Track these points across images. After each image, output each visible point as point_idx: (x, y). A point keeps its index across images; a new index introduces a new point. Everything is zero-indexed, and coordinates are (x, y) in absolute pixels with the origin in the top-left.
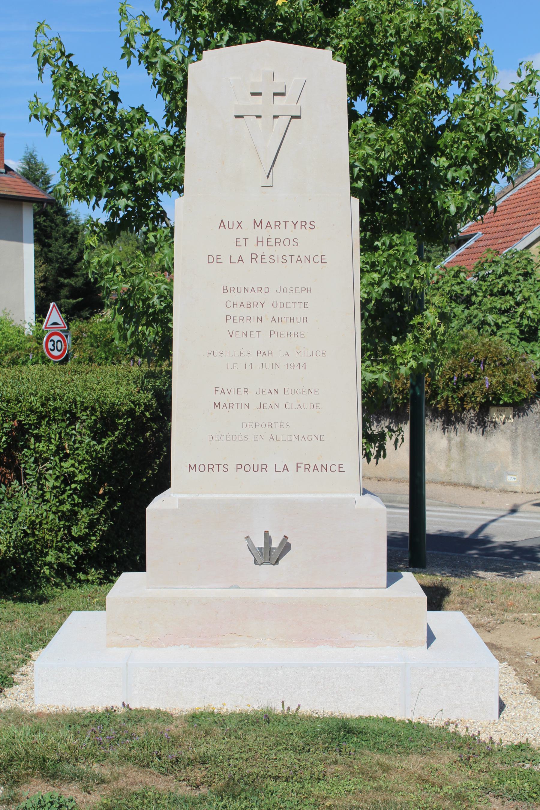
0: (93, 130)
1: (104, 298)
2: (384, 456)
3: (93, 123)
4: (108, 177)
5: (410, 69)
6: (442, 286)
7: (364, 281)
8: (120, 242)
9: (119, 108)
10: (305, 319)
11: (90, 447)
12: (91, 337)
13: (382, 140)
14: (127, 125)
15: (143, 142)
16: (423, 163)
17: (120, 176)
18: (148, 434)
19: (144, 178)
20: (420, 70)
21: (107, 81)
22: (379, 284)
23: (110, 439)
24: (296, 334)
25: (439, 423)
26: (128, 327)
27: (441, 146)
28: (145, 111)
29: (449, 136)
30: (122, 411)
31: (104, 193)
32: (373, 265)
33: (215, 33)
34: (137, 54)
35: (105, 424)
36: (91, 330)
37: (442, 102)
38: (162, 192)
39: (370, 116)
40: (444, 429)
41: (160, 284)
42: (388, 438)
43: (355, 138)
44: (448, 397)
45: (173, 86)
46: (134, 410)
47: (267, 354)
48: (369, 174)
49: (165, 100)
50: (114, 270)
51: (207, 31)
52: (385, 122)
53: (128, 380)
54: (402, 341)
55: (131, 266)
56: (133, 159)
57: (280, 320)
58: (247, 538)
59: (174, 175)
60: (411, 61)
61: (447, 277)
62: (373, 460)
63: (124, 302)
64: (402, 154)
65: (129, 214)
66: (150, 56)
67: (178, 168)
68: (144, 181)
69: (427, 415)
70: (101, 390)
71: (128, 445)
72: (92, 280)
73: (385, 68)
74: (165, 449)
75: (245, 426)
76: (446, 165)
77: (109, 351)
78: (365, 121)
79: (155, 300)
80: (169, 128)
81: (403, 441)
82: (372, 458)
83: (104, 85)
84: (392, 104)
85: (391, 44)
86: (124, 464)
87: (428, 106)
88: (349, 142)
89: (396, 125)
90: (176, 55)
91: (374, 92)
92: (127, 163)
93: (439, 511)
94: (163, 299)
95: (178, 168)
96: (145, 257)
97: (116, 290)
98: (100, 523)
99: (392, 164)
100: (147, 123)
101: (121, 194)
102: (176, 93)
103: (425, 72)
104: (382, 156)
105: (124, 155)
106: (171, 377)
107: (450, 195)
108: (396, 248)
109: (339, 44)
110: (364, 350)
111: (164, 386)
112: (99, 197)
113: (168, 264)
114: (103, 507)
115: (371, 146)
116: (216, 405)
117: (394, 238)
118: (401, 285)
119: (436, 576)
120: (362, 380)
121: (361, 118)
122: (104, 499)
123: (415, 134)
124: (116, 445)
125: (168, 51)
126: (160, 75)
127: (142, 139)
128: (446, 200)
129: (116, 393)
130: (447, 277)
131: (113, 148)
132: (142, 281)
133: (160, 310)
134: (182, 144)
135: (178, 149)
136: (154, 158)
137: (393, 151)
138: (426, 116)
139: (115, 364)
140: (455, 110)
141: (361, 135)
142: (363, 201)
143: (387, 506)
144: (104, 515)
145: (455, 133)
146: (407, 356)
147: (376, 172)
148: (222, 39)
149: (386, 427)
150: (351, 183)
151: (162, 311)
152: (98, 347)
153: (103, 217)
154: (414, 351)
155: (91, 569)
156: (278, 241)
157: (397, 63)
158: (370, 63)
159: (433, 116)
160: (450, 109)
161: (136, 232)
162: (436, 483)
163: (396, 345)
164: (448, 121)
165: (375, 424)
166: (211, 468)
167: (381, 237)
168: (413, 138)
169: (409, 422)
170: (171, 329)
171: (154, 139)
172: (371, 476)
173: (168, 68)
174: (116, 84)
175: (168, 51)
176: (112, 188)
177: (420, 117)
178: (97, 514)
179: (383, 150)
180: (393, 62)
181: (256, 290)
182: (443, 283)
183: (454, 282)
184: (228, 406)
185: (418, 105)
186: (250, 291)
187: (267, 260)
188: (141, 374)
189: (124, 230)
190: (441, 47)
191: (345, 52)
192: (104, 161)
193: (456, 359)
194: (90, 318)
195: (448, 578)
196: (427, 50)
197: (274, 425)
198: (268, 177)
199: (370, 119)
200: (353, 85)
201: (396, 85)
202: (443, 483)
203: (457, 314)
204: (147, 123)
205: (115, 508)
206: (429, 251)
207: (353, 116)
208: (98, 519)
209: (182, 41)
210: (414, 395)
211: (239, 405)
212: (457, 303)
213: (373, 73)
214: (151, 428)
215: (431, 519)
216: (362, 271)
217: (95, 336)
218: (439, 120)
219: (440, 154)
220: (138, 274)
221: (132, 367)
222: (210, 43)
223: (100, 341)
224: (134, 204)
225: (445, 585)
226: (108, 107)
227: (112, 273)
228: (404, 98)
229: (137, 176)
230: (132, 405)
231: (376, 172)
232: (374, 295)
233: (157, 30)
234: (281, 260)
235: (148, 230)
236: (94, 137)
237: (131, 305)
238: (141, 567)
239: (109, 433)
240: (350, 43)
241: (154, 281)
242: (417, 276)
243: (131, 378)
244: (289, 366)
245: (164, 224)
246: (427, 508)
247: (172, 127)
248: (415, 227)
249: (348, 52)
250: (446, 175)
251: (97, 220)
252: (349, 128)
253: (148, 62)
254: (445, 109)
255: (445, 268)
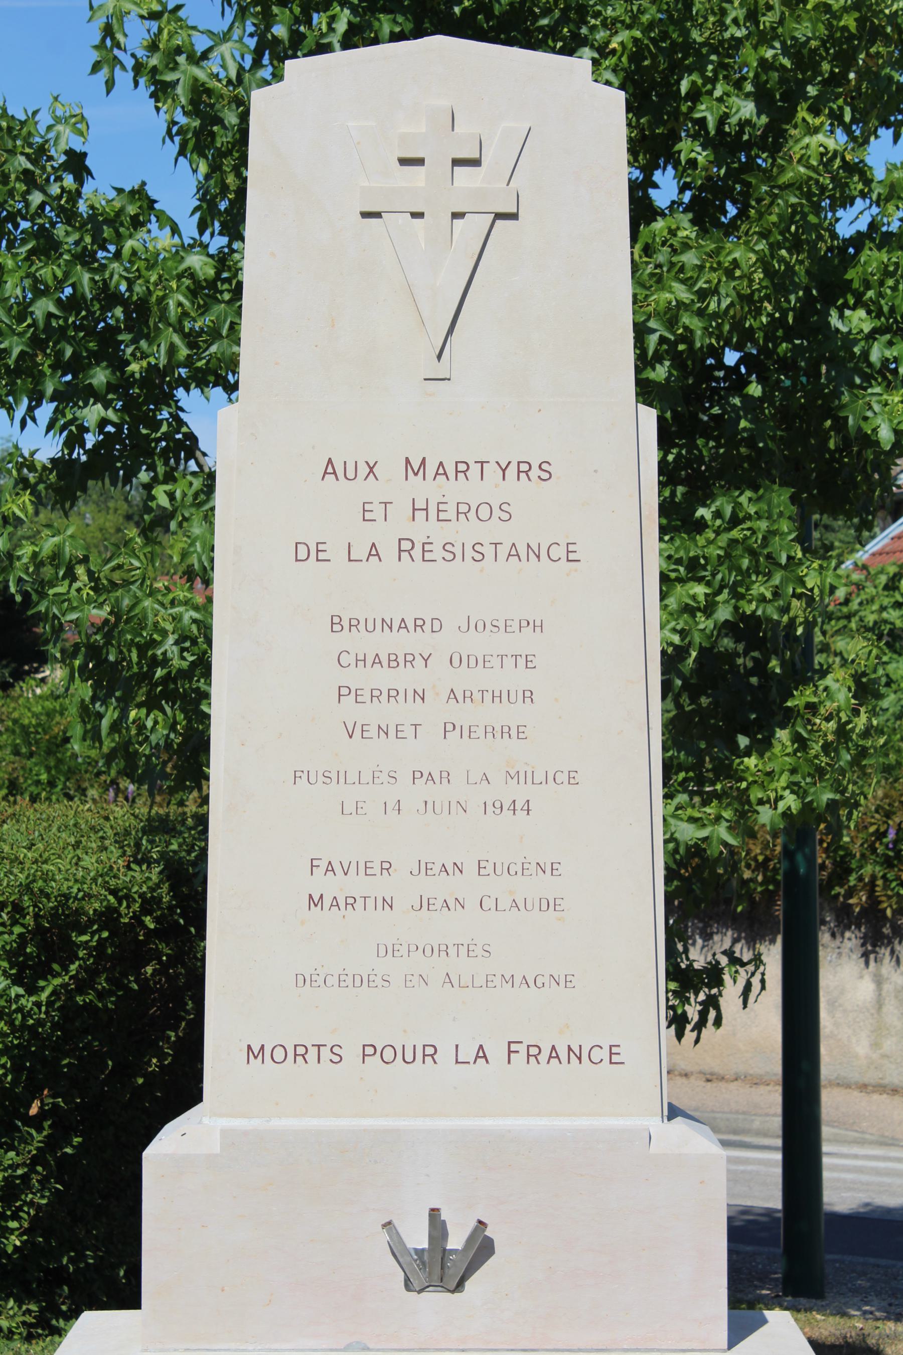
0: (24, 242)
1: (47, 642)
2: (718, 1022)
3: (25, 225)
4: (59, 354)
5: (780, 101)
6: (857, 612)
7: (672, 602)
8: (86, 503)
9: (88, 188)
10: (528, 696)
11: (9, 1001)
12: (13, 732)
13: (712, 269)
14: (107, 232)
15: (144, 272)
16: (810, 323)
17: (87, 350)
18: (149, 970)
19: (145, 356)
20: (805, 105)
21: (60, 128)
22: (709, 609)
23: (57, 981)
24: (505, 732)
25: (852, 940)
26: (102, 710)
27: (856, 285)
28: (148, 197)
29: (873, 259)
30: (86, 914)
31: (49, 390)
32: (693, 565)
33: (315, 16)
34: (129, 63)
35: (45, 946)
36: (16, 715)
37: (856, 178)
38: (188, 390)
39: (685, 211)
40: (866, 955)
41: (181, 609)
42: (727, 978)
43: (647, 263)
44: (873, 878)
45: (216, 139)
46: (116, 910)
47: (437, 778)
48: (681, 347)
49: (195, 171)
50: (71, 576)
51: (297, 10)
52: (719, 225)
53: (102, 838)
54: (762, 746)
55: (113, 564)
56: (119, 312)
57: (468, 696)
58: (388, 1225)
59: (214, 349)
60: (782, 81)
61: (870, 590)
62: (690, 1035)
63: (94, 652)
64: (761, 300)
65: (109, 440)
66: (160, 67)
67: (224, 332)
68: (144, 364)
69: (823, 922)
70: (36, 862)
71: (101, 995)
72: (18, 598)
73: (720, 100)
74: (190, 1005)
75: (382, 952)
76: (867, 328)
77: (56, 767)
78: (671, 222)
79: (169, 646)
80: (206, 238)
81: (763, 988)
82: (689, 1027)
83: (51, 135)
84: (735, 183)
85: (737, 43)
86: (90, 1043)
87: (823, 189)
88: (634, 272)
89: (747, 234)
90: (224, 66)
91: (693, 155)
92: (105, 321)
93: (856, 1157)
94: (187, 644)
95: (224, 332)
96: (146, 545)
97: (76, 623)
98: (30, 1188)
99: (737, 325)
100: (154, 226)
101: (91, 394)
102: (222, 154)
103: (815, 110)
104: (713, 306)
105: (99, 301)
106: (206, 830)
107: (879, 402)
108: (748, 524)
109: (608, 43)
110: (669, 768)
111: (189, 853)
112: (37, 399)
113: (200, 560)
114: (38, 1149)
115: (688, 282)
116: (314, 902)
117: (743, 499)
118: (759, 612)
119: (851, 1317)
120: (666, 842)
121: (663, 215)
122: (40, 1130)
123: (791, 254)
124: (70, 995)
125: (205, 55)
126: (185, 113)
127: (143, 264)
128: (869, 414)
129: (73, 870)
130: (870, 590)
131: (73, 286)
132: (137, 602)
133: (180, 671)
134: (236, 275)
135: (226, 286)
136: (166, 308)
137: (739, 295)
138: (817, 215)
139: (70, 798)
140: (888, 200)
141: (662, 256)
142: (668, 415)
143: (725, 1144)
144: (39, 1169)
145: (888, 252)
146: (774, 781)
147: (698, 345)
148: (331, 29)
149: (724, 953)
150: (638, 370)
151: (186, 674)
152: (31, 755)
153: (46, 447)
154: (793, 771)
155: (6, 1300)
156: (463, 508)
157: (749, 88)
158: (684, 86)
159: (834, 211)
160: (874, 197)
161: (124, 485)
162: (848, 1086)
163: (749, 756)
164: (873, 226)
165: (700, 942)
166: (300, 1053)
167: (712, 497)
168: (787, 264)
169: (779, 939)
170: (208, 717)
171: (170, 263)
172: (688, 1068)
173: (204, 97)
174: (81, 134)
175: (205, 55)
176: (69, 378)
177: (804, 216)
178: (24, 1164)
179: (715, 291)
180: (738, 85)
181: (411, 626)
182: (861, 604)
183: (886, 601)
184: (342, 904)
185: (800, 188)
186: (395, 627)
187: (438, 553)
188: (133, 821)
189: (95, 478)
190: (856, 51)
191: (624, 59)
192: (50, 315)
193: (893, 787)
194: (12, 686)
195: (879, 1324)
196: (820, 55)
197: (452, 951)
198: (439, 357)
199: (684, 219)
200: (644, 138)
201: (746, 137)
202: (863, 1087)
203: (894, 677)
204: (154, 226)
205: (68, 1150)
206: (827, 527)
207: (642, 210)
208: (25, 1178)
209: (236, 33)
210: (792, 873)
211: (370, 903)
212: (895, 652)
213: (691, 109)
214: (158, 955)
215: (835, 1175)
216: (664, 578)
217: (25, 729)
218: (850, 221)
219: (852, 302)
220: (127, 583)
221: (113, 806)
222: (303, 37)
223: (37, 742)
224: (122, 418)
225: (871, 1341)
226: (62, 188)
227: (66, 583)
228: (765, 171)
229: (129, 351)
230: (111, 898)
231: (698, 345)
232: (697, 638)
233: (179, 7)
234: (469, 553)
235: (155, 480)
236: (27, 259)
237: (112, 658)
238: (127, 1296)
239: (56, 967)
240: (635, 40)
241: (167, 600)
242: (799, 591)
243: (110, 833)
244: (490, 808)
245: (192, 466)
246: (825, 1148)
247: (212, 235)
248: (793, 475)
249: (630, 60)
250: (866, 354)
251: (33, 454)
252: (634, 237)
253: (155, 83)
254: (863, 195)
255: (865, 567)
